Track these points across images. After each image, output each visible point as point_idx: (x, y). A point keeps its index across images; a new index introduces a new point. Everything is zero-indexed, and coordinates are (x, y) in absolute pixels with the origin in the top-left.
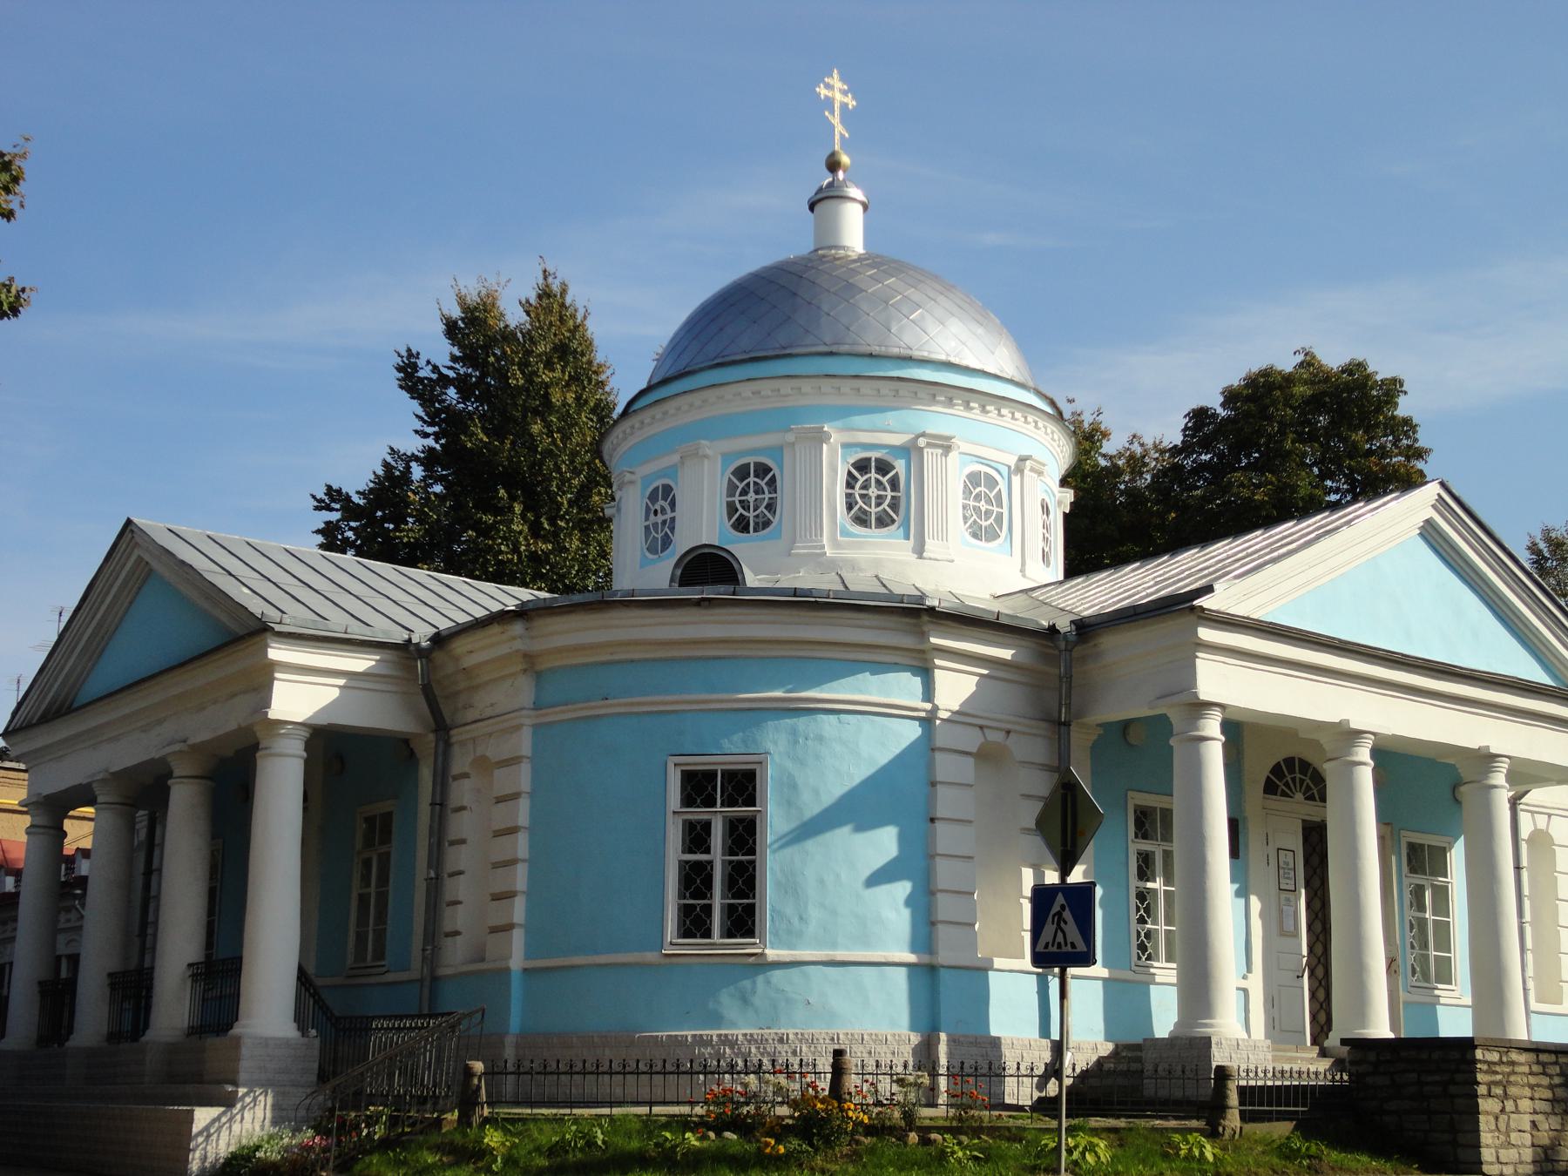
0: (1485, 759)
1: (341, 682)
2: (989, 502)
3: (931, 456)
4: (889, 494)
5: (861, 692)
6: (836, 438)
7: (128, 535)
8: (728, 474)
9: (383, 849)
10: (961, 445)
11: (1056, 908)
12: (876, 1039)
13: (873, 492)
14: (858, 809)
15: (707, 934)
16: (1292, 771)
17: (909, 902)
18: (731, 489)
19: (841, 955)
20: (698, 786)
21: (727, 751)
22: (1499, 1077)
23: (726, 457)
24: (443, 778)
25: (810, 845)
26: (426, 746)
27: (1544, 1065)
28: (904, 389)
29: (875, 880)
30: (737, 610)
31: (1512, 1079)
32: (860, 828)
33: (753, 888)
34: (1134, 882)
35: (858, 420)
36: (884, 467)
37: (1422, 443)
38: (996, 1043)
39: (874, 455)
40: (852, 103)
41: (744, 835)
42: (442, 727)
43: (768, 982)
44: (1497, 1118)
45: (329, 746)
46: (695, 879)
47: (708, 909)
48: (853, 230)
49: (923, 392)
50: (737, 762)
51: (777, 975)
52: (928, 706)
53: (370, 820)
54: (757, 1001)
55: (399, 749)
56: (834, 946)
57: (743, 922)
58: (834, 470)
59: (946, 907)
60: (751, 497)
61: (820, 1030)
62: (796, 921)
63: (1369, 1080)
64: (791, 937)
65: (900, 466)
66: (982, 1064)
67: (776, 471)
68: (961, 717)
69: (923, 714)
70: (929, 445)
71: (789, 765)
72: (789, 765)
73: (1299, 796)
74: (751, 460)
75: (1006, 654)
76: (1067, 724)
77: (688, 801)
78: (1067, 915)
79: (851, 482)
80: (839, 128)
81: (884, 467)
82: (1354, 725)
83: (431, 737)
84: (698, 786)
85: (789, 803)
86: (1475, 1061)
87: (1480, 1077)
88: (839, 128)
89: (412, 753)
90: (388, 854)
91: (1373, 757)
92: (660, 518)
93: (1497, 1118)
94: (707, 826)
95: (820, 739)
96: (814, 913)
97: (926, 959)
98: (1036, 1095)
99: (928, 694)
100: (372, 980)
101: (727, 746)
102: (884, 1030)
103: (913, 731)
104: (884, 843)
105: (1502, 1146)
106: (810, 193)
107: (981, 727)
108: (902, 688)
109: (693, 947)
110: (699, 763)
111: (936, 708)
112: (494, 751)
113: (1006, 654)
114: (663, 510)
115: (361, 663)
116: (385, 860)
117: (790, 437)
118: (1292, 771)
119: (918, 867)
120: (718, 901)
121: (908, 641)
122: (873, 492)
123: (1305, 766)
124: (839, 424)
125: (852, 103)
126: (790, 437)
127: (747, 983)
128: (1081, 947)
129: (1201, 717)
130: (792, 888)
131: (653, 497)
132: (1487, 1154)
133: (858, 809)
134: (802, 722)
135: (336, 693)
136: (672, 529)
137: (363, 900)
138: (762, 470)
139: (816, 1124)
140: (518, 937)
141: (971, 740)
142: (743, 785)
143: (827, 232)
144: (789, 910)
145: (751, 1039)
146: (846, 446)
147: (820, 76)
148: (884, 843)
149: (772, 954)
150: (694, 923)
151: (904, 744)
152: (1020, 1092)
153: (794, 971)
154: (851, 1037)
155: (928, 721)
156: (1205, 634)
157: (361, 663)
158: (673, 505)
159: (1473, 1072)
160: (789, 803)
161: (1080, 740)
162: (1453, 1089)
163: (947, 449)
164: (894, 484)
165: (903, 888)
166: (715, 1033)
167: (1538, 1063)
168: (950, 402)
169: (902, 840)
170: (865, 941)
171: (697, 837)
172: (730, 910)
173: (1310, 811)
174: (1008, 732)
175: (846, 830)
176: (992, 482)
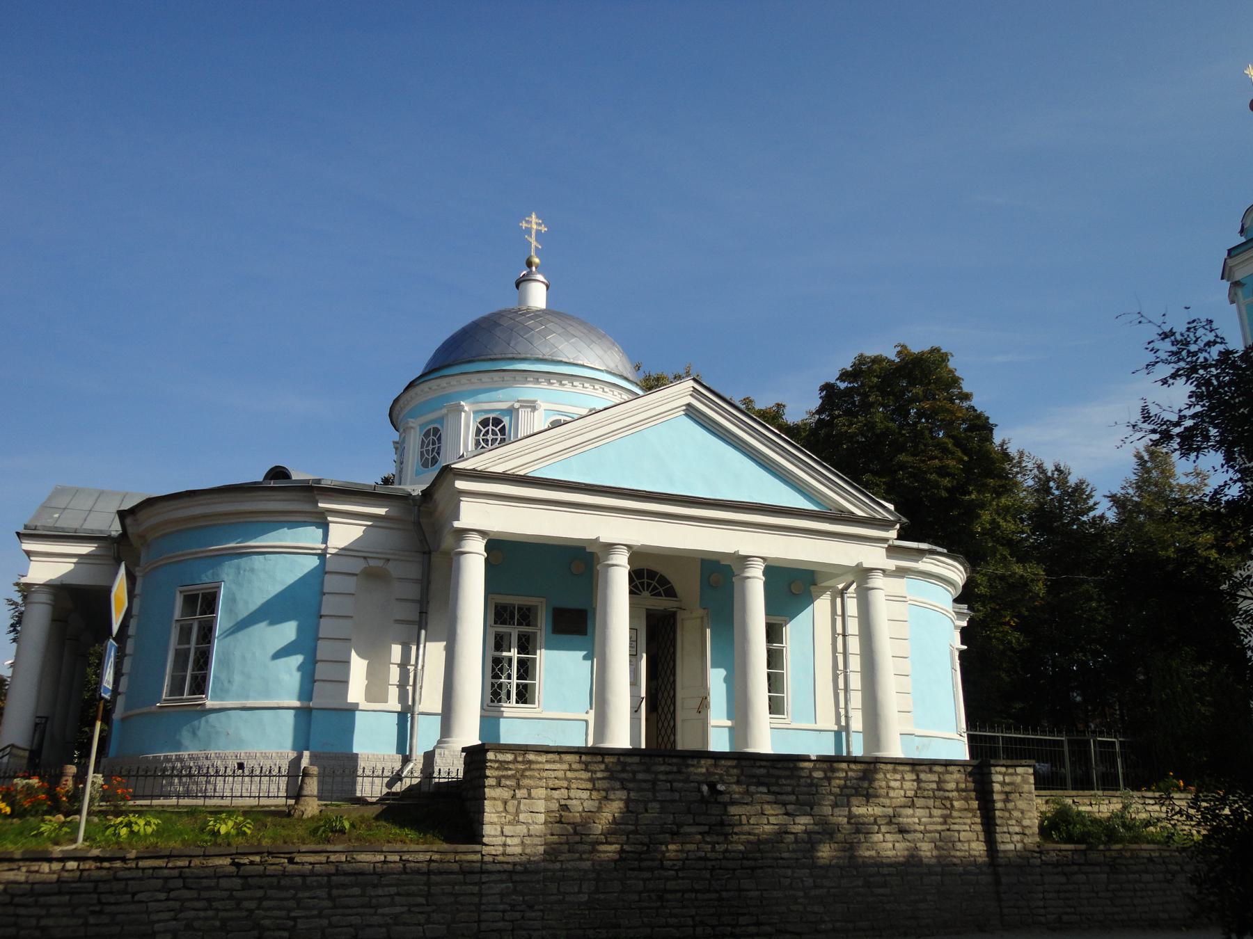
1: (75, 560)
3: (523, 414)
5: (280, 540)
10: (543, 406)
12: (265, 756)
14: (272, 612)
17: (300, 668)
19: (250, 703)
22: (510, 773)
23: (421, 426)
25: (240, 635)
27: (586, 764)
28: (507, 376)
29: (278, 655)
31: (527, 773)
32: (272, 623)
35: (482, 397)
36: (497, 422)
37: (966, 388)
38: (355, 757)
39: (491, 416)
40: (544, 229)
41: (207, 633)
43: (207, 721)
44: (505, 803)
48: (537, 296)
49: (519, 376)
51: (213, 716)
52: (323, 546)
54: (200, 733)
56: (247, 698)
57: (200, 686)
58: (467, 426)
59: (322, 671)
61: (230, 752)
62: (226, 684)
64: (222, 693)
65: (506, 421)
66: (340, 768)
68: (345, 552)
70: (522, 407)
71: (233, 587)
72: (233, 587)
75: (382, 511)
76: (430, 553)
79: (478, 432)
80: (534, 244)
81: (497, 422)
82: (866, 565)
84: (190, 600)
85: (231, 611)
86: (485, 761)
87: (488, 773)
88: (534, 244)
91: (765, 573)
93: (505, 803)
95: (252, 570)
96: (237, 678)
97: (305, 704)
98: (385, 790)
99: (325, 539)
101: (205, 579)
102: (272, 750)
103: (314, 562)
104: (288, 631)
105: (510, 823)
107: (365, 558)
108: (309, 536)
113: (382, 511)
115: (85, 549)
117: (444, 411)
119: (306, 645)
121: (307, 507)
124: (471, 400)
125: (544, 229)
126: (444, 411)
127: (196, 723)
129: (462, 539)
130: (226, 663)
132: (488, 830)
133: (272, 612)
134: (243, 561)
135: (72, 566)
141: (357, 566)
142: (209, 602)
143: (522, 298)
144: (223, 676)
145: (191, 758)
146: (475, 412)
147: (524, 216)
148: (288, 631)
149: (209, 703)
151: (306, 571)
152: (370, 788)
153: (222, 714)
154: (249, 756)
155: (322, 556)
156: (460, 484)
157: (85, 549)
159: (485, 768)
160: (231, 611)
163: (534, 409)
164: (503, 430)
165: (299, 659)
166: (173, 754)
167: (580, 762)
168: (537, 381)
169: (300, 630)
170: (266, 694)
171: (185, 633)
172: (194, 678)
174: (388, 560)
175: (263, 624)
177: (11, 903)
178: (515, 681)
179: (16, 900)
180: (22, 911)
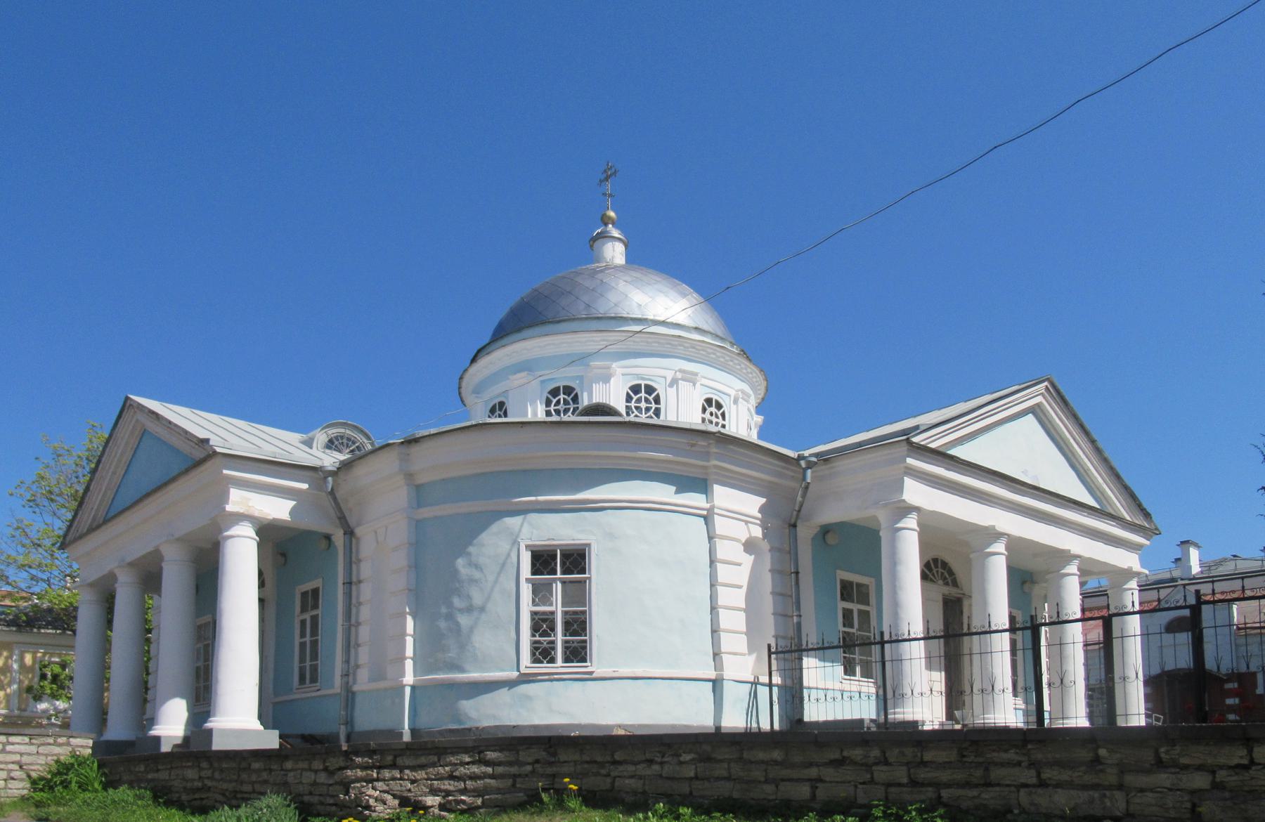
4: (654, 406)
6: (619, 371)
9: (314, 613)
13: (643, 405)
15: (552, 660)
16: (936, 567)
20: (543, 560)
26: (339, 538)
33: (584, 629)
45: (268, 533)
46: (542, 624)
53: (304, 595)
69: (705, 513)
73: (941, 582)
84: (543, 560)
91: (1007, 549)
100: (500, 770)
107: (747, 522)
109: (544, 668)
111: (713, 508)
118: (936, 567)
120: (559, 637)
123: (945, 565)
137: (303, 645)
138: (568, 390)
139: (1049, 816)
140: (409, 664)
142: (576, 559)
150: (543, 653)
161: (805, 532)
172: (567, 646)
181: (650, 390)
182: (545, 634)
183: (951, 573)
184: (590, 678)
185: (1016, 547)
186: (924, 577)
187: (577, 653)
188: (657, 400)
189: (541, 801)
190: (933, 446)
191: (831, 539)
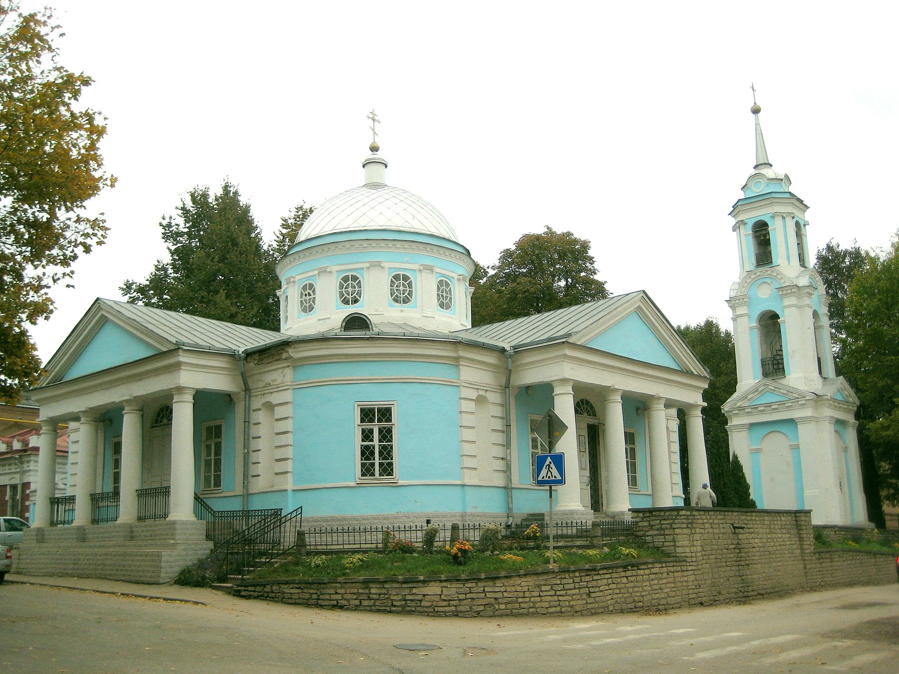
0: (651, 397)
2: (306, 300)
7: (97, 305)
8: (340, 280)
9: (217, 440)
11: (547, 463)
13: (401, 288)
15: (373, 475)
18: (341, 286)
20: (367, 414)
21: (376, 397)
24: (247, 411)
30: (360, 342)
34: (531, 450)
41: (386, 435)
42: (247, 389)
46: (367, 453)
47: (373, 465)
50: (383, 404)
55: (228, 398)
60: (350, 289)
63: (640, 524)
67: (361, 278)
73: (586, 414)
74: (350, 274)
77: (362, 421)
78: (552, 465)
83: (243, 393)
84: (367, 414)
89: (231, 400)
90: (220, 443)
92: (308, 298)
94: (371, 431)
106: (363, 160)
110: (368, 404)
112: (275, 399)
114: (310, 295)
116: (218, 446)
122: (401, 288)
123: (588, 402)
128: (559, 477)
131: (304, 288)
136: (314, 302)
142: (385, 414)
150: (367, 470)
158: (314, 291)
162: (674, 526)
171: (367, 435)
173: (592, 421)
176: (447, 285)
177: (555, 595)
178: (377, 462)
179: (558, 593)
180: (560, 598)
181: (406, 278)
182: (367, 459)
183: (592, 407)
184: (395, 485)
185: (578, 388)
186: (576, 412)
187: (387, 469)
188: (410, 285)
189: (559, 253)
190: (579, 343)
191: (529, 392)
